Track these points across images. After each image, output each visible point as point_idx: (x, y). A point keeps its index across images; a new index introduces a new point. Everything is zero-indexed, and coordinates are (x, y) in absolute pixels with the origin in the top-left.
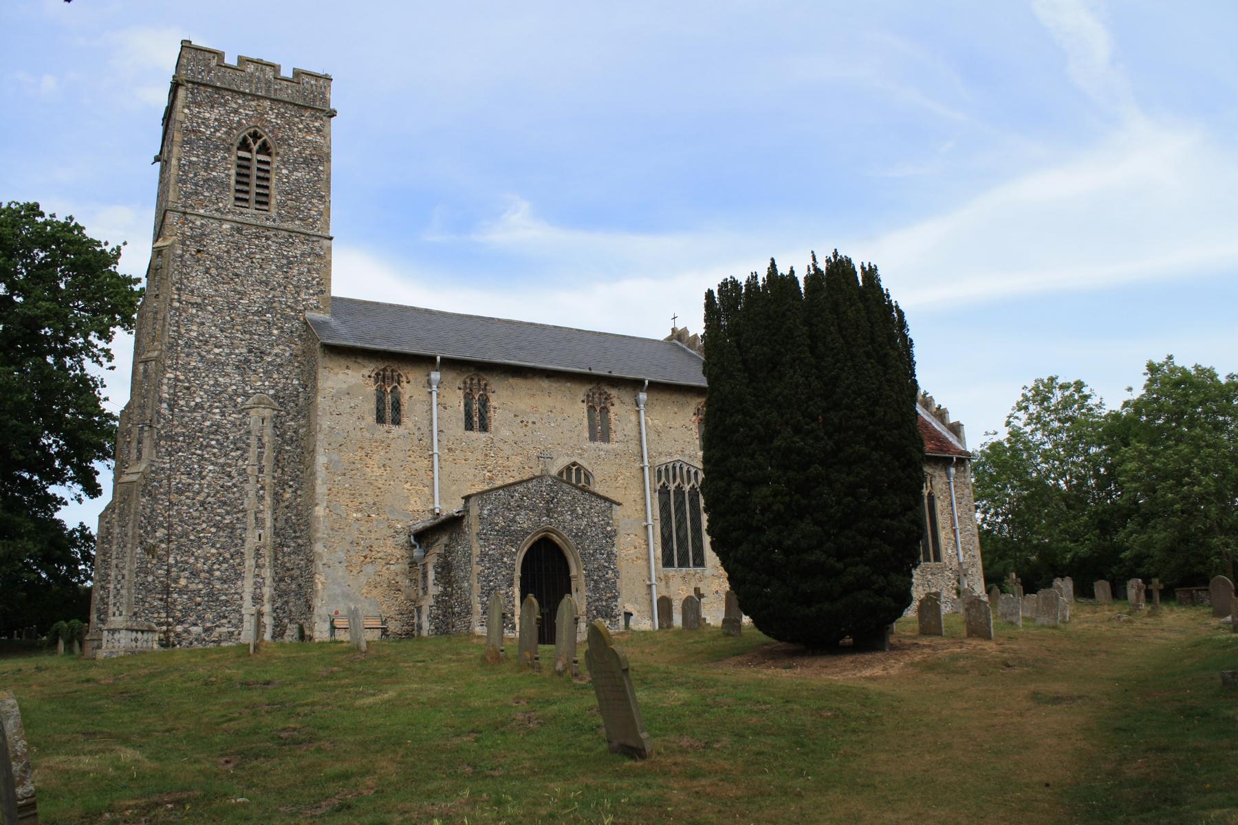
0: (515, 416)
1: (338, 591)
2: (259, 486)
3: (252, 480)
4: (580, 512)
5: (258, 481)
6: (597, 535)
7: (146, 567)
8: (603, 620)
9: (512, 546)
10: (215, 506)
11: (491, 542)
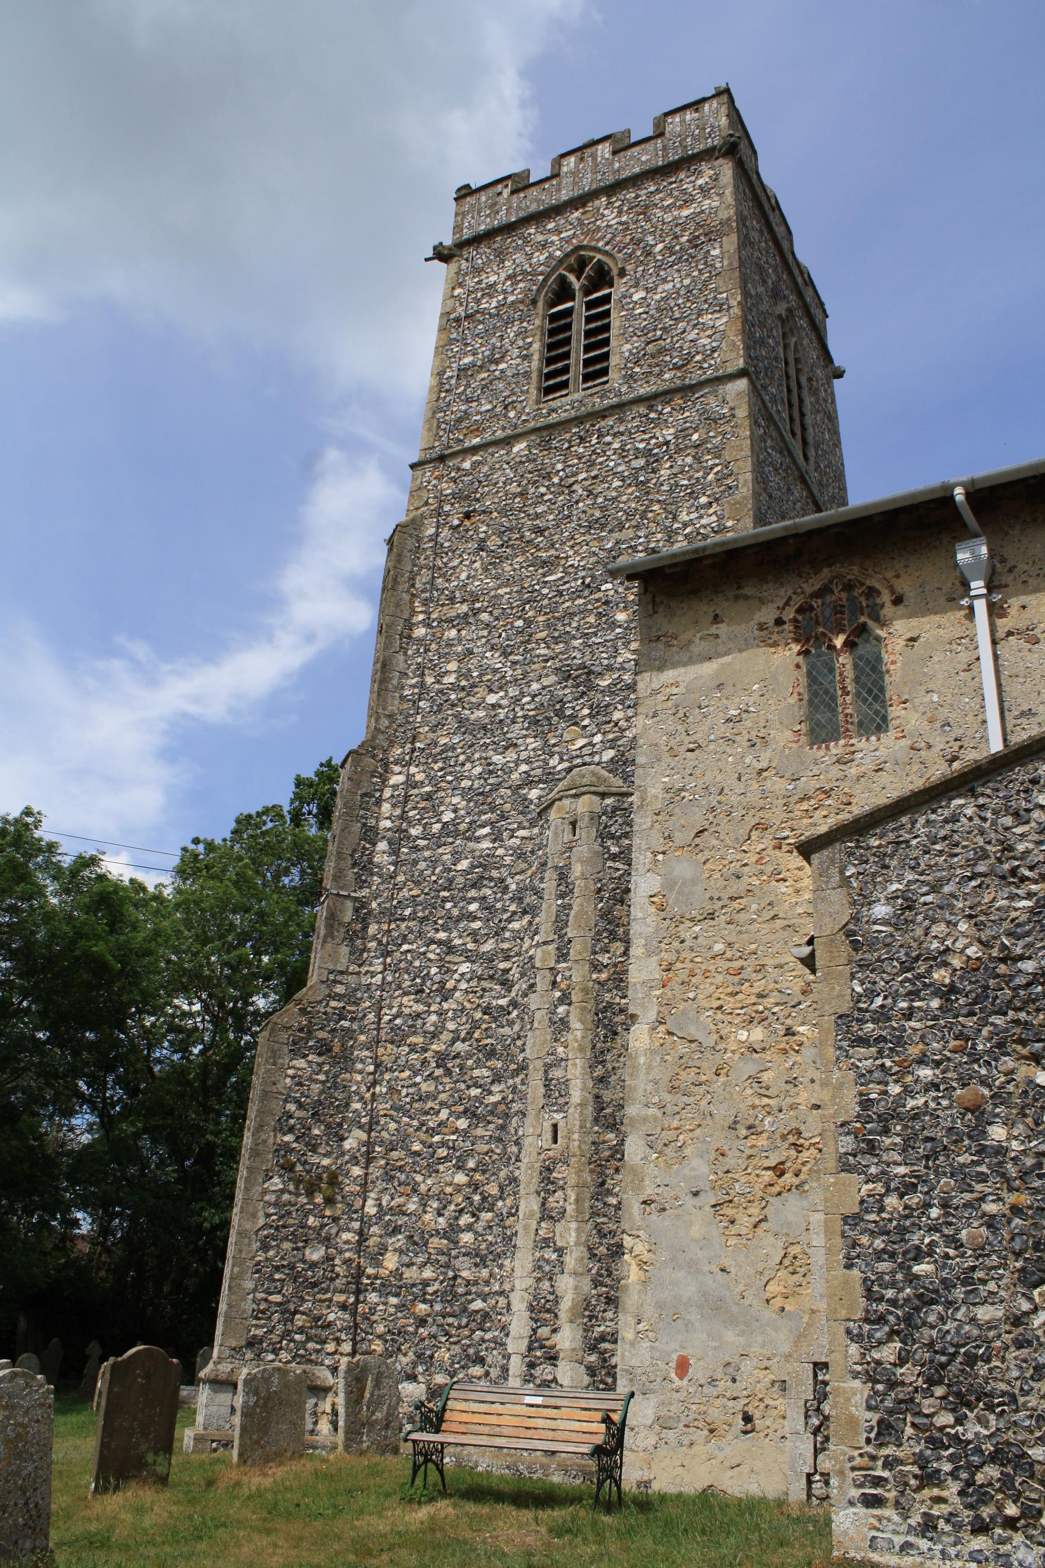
1: (690, 1290)
2: (558, 994)
3: (542, 981)
5: (554, 983)
7: (303, 1226)
10: (470, 1062)
11: (914, 1051)
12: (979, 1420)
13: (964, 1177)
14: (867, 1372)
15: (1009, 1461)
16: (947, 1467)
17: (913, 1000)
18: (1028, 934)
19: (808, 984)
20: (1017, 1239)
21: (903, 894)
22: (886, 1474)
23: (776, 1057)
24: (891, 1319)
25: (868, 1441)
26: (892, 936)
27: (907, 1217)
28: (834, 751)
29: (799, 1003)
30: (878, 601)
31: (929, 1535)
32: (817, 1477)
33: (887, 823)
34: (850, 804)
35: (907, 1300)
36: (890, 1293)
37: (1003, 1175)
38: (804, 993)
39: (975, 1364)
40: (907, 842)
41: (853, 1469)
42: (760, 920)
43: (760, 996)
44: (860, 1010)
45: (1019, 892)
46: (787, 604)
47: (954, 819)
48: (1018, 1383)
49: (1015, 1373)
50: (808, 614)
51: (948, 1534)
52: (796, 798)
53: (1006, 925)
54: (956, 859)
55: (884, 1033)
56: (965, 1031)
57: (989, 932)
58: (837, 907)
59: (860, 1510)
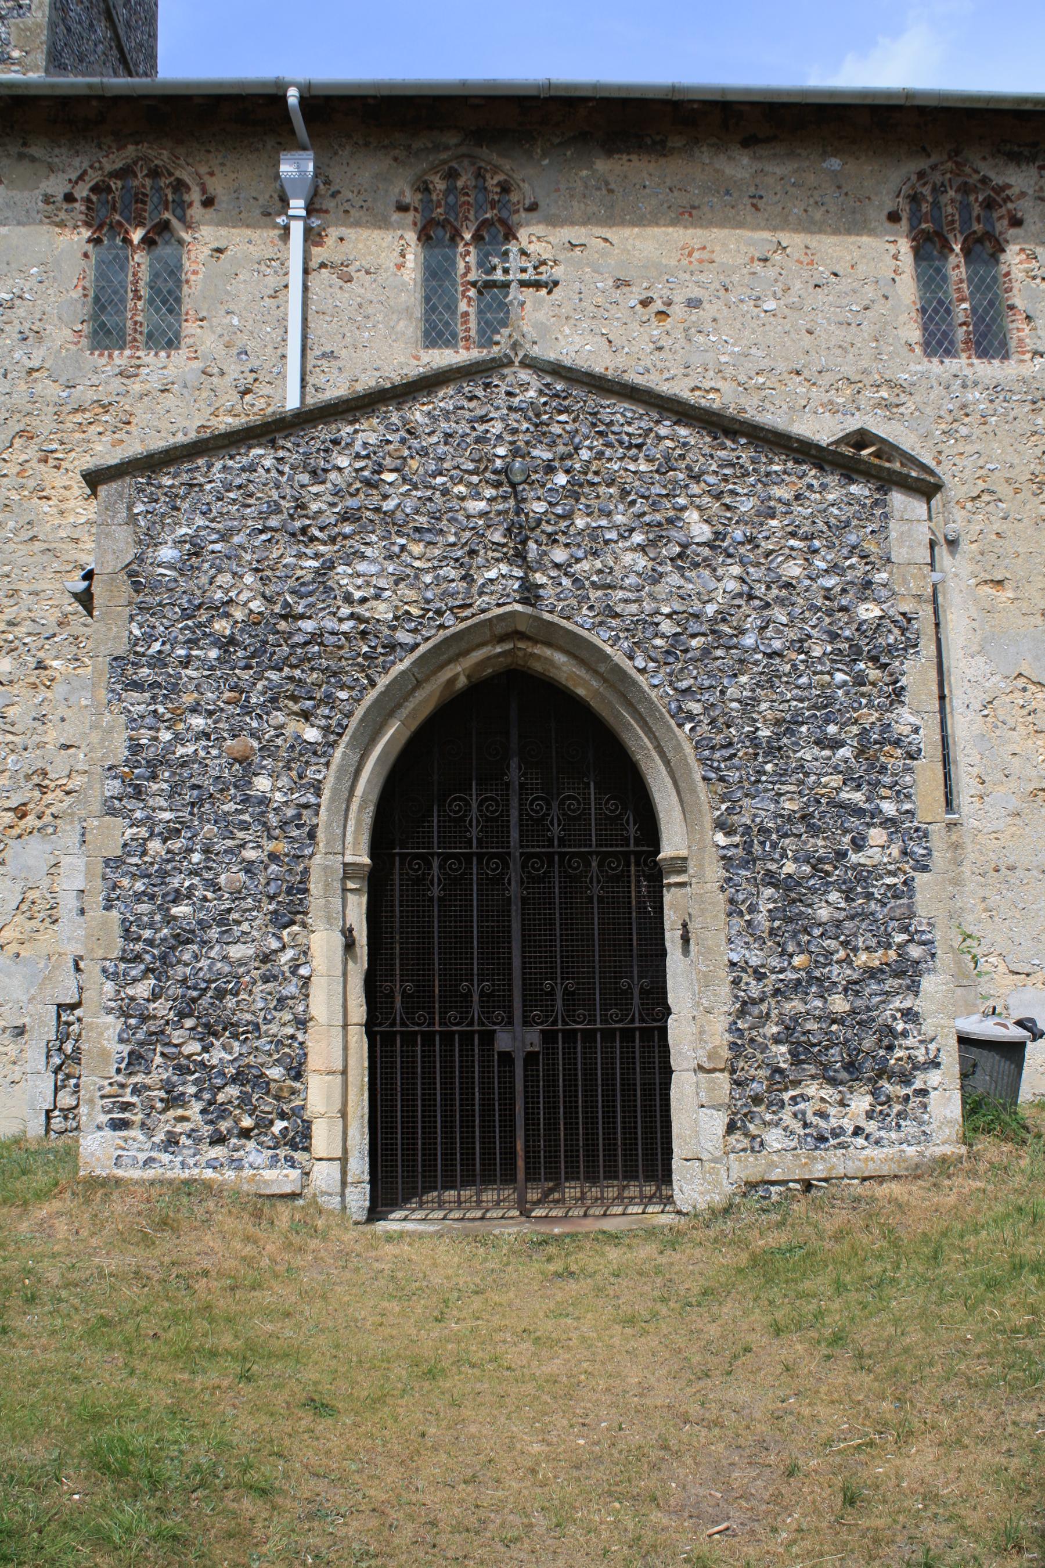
0: (621, 283)
4: (702, 532)
6: (800, 645)
8: (828, 1092)
9: (306, 716)
11: (188, 699)
12: (224, 1047)
13: (227, 825)
14: (121, 1008)
15: (248, 1082)
16: (192, 1090)
17: (191, 649)
18: (310, 594)
19: (66, 616)
20: (272, 884)
21: (192, 540)
22: (134, 1099)
23: (24, 691)
24: (148, 958)
25: (118, 1071)
26: (176, 581)
27: (168, 861)
28: (118, 361)
29: (54, 635)
30: (186, 197)
31: (171, 1149)
32: (57, 1113)
33: (183, 463)
34: (129, 423)
35: (164, 940)
36: (147, 934)
37: (264, 824)
38: (60, 624)
39: (224, 997)
40: (201, 485)
41: (103, 1097)
42: (16, 539)
43: (11, 623)
44: (136, 653)
45: (307, 551)
46: (81, 178)
47: (251, 468)
48: (262, 1013)
49: (260, 1005)
50: (104, 195)
51: (189, 1147)
52: (69, 408)
53: (291, 583)
54: (249, 510)
55: (159, 679)
56: (241, 683)
57: (273, 587)
58: (121, 545)
59: (108, 1133)
